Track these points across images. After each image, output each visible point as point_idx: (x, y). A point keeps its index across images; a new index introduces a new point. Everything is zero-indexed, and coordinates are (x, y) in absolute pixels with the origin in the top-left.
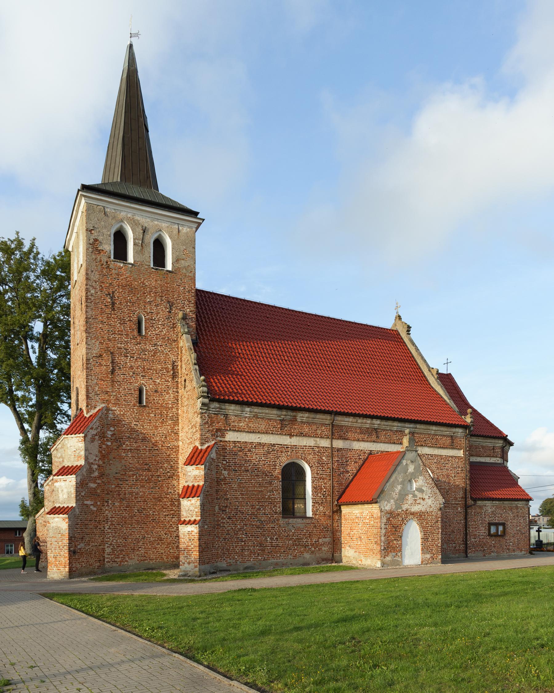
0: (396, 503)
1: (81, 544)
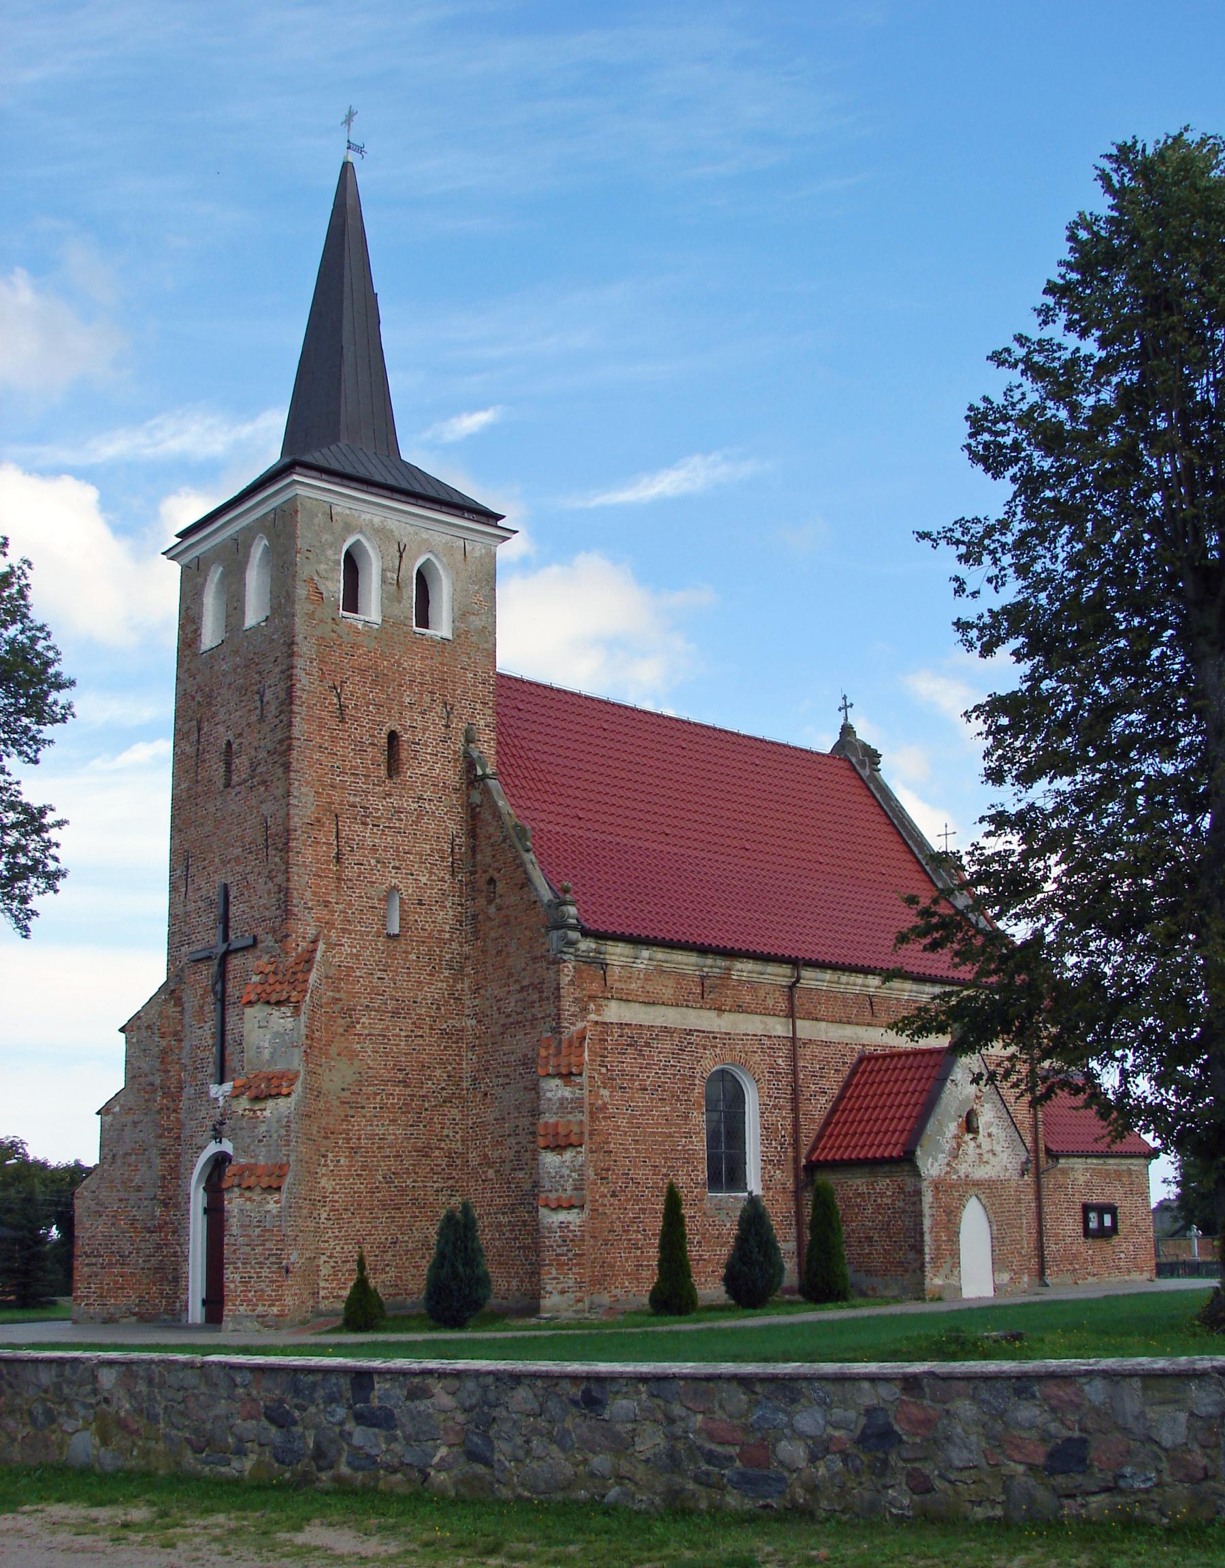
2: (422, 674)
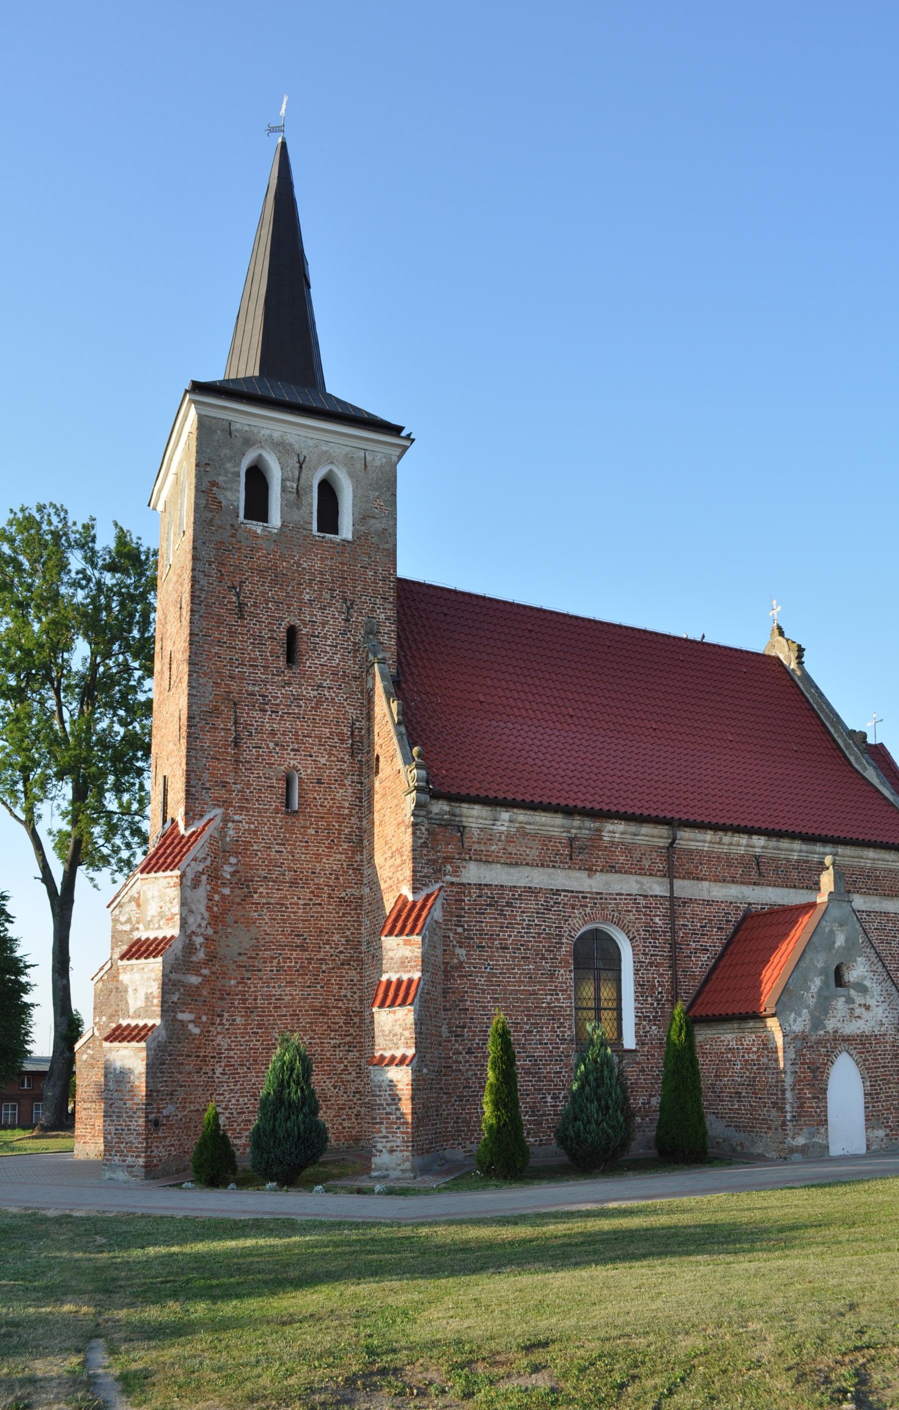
1: (170, 1106)
2: (321, 573)
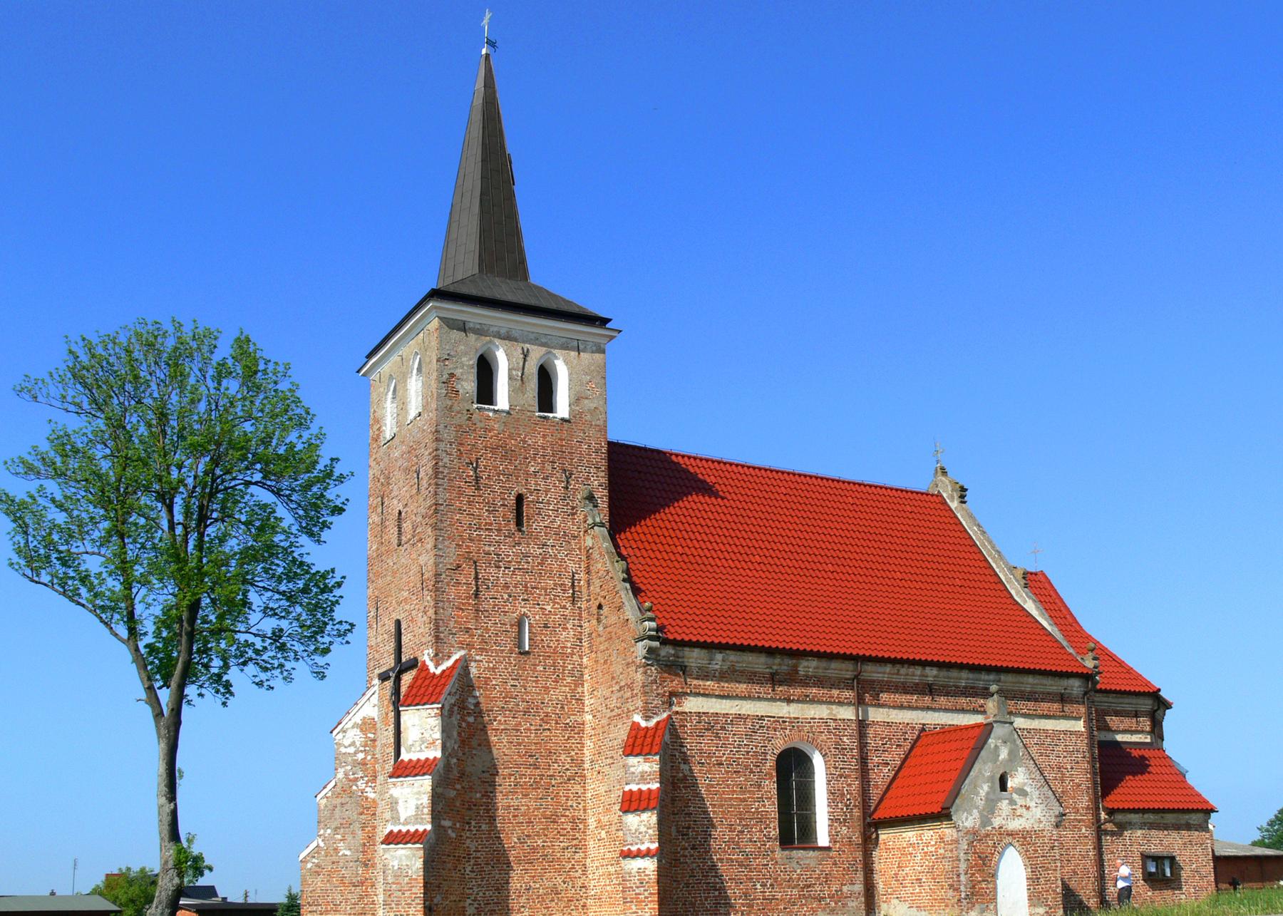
0: (982, 816)
